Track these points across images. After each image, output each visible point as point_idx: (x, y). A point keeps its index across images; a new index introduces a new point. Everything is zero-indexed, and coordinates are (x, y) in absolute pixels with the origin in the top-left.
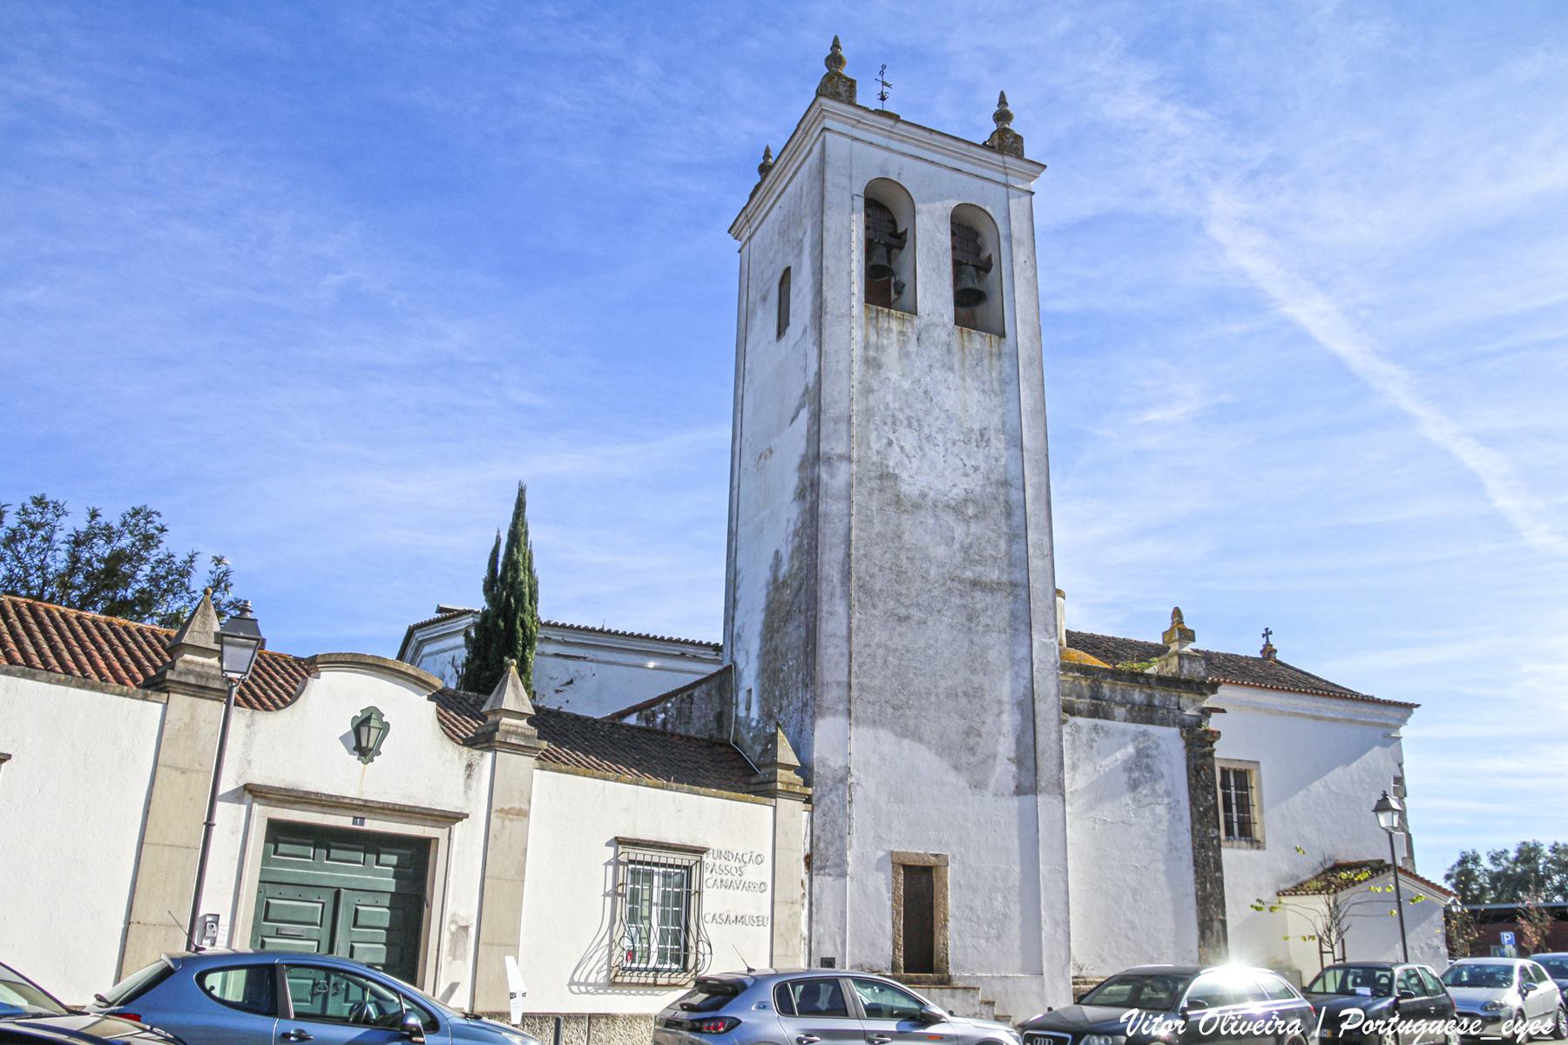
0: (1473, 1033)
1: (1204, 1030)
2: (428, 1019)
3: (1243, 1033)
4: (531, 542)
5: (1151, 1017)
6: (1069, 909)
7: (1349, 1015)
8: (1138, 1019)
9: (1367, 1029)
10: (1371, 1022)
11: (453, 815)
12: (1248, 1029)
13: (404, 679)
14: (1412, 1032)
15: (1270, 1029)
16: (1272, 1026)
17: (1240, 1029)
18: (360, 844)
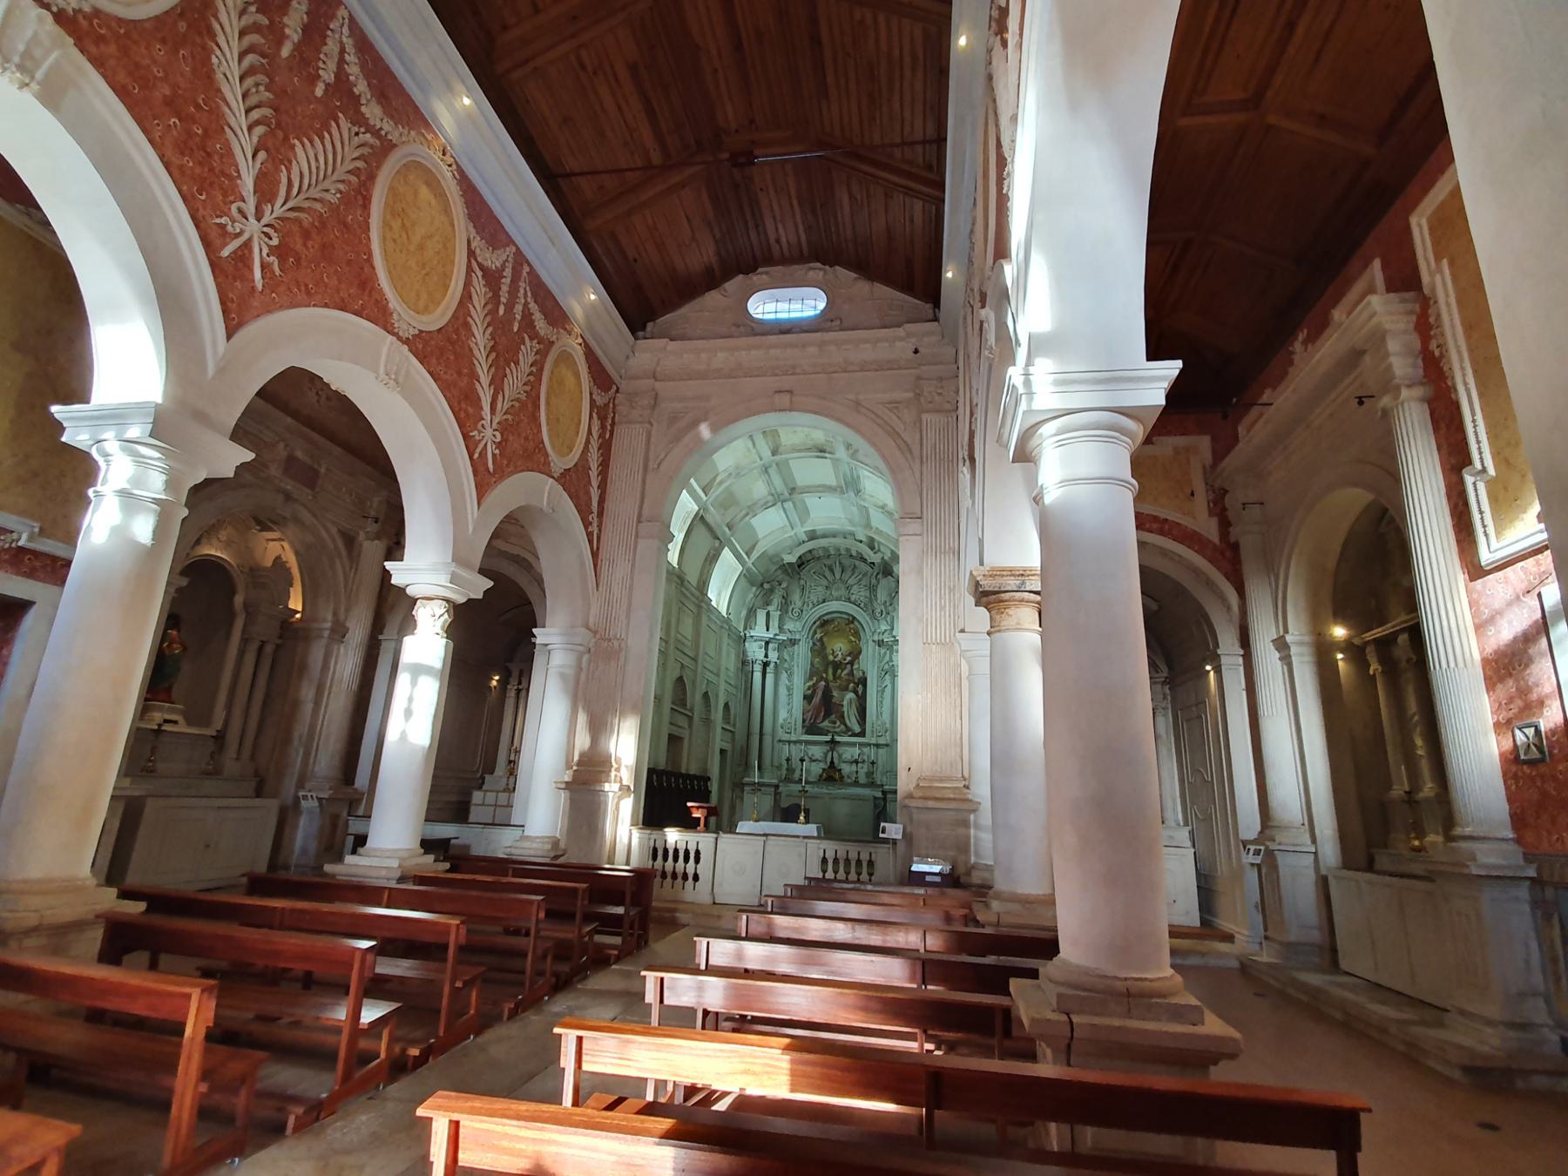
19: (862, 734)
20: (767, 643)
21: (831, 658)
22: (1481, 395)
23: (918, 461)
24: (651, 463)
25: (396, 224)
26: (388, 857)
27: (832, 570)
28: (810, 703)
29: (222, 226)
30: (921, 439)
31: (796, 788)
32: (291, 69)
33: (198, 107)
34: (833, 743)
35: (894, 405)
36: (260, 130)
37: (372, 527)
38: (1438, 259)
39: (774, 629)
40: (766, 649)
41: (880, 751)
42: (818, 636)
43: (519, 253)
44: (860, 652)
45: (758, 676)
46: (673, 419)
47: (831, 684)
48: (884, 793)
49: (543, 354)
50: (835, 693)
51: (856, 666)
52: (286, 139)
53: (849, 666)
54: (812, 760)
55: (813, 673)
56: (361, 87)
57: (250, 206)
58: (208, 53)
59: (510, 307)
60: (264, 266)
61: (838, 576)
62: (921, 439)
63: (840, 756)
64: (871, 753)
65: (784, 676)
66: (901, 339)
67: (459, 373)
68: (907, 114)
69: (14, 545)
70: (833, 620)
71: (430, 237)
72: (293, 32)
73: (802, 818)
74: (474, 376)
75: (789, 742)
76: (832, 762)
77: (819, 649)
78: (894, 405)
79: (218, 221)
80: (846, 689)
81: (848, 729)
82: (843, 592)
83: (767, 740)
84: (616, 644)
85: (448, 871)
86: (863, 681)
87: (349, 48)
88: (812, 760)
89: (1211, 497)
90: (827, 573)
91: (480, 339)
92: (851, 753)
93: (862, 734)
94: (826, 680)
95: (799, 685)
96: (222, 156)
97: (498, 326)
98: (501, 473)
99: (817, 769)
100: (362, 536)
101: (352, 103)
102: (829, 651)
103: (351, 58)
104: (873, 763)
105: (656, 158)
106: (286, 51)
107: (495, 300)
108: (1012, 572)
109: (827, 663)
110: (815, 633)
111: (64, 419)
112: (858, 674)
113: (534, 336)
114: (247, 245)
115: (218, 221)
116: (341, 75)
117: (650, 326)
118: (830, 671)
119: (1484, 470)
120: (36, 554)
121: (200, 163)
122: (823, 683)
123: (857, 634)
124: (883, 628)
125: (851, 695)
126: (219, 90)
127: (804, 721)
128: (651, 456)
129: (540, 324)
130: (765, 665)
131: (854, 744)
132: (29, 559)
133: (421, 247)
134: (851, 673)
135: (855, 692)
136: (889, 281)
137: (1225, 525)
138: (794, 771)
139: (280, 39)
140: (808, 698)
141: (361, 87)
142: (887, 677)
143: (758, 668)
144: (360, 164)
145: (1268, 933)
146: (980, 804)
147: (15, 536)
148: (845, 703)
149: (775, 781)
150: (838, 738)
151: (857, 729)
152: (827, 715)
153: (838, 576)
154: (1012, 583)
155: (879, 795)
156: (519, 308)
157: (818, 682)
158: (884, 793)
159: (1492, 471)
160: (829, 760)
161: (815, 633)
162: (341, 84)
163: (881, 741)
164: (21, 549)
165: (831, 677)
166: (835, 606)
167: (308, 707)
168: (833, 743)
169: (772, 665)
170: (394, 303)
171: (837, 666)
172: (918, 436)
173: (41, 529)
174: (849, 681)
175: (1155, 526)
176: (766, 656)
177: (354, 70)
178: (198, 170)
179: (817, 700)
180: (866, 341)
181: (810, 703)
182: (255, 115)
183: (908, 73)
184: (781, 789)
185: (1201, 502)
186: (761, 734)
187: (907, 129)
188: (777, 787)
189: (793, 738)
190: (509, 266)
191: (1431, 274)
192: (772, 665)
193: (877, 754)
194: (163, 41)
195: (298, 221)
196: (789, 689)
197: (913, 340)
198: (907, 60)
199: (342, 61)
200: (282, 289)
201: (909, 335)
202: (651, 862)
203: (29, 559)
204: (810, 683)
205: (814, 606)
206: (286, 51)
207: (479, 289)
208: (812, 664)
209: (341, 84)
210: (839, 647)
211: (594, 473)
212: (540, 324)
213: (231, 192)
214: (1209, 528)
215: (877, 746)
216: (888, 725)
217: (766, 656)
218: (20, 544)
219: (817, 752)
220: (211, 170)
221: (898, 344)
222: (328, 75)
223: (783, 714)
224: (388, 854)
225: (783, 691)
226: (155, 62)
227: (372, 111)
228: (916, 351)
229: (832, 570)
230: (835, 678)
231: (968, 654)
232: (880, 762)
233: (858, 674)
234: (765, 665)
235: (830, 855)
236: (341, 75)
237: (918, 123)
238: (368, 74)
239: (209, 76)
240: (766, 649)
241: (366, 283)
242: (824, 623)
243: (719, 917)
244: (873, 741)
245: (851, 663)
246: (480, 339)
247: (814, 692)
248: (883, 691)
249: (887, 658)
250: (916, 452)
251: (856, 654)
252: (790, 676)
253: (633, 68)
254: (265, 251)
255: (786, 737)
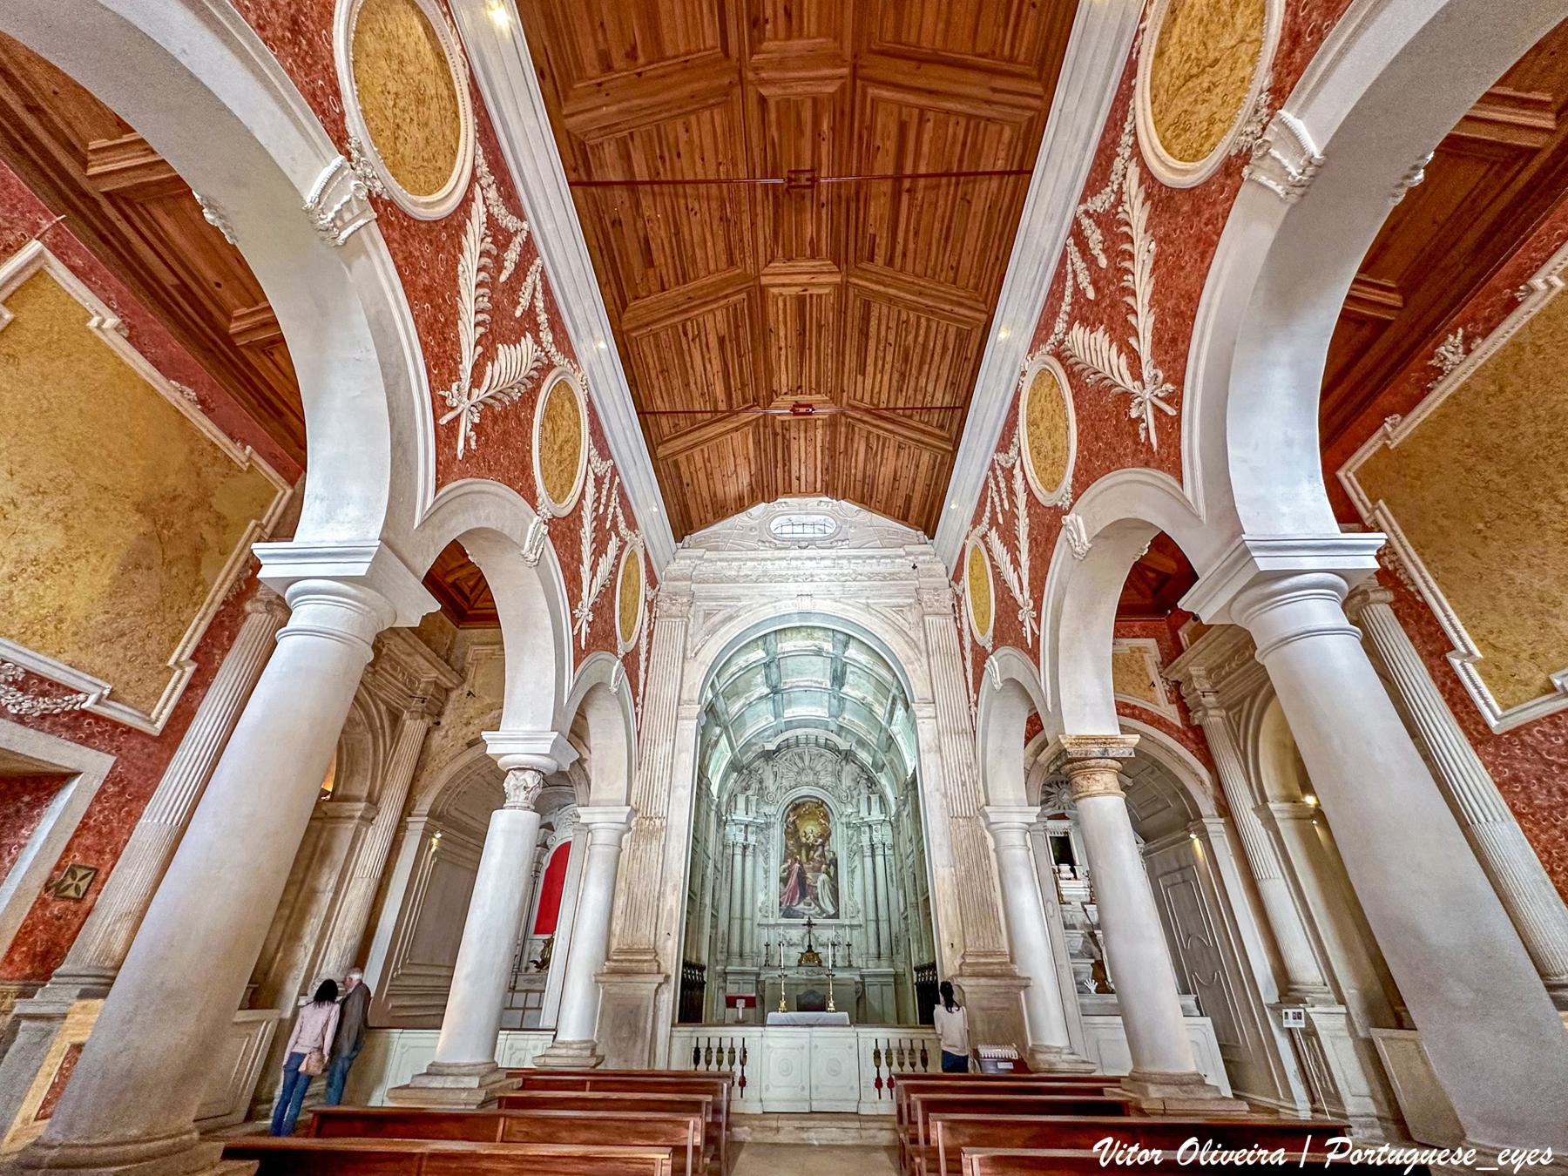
0: (1467, 1163)
1: (1183, 1161)
2: (669, 1149)
3: (1224, 1163)
4: (1027, 326)
5: (1125, 1146)
6: (1538, 970)
7: (1335, 1144)
8: (1112, 1147)
9: (1355, 1158)
10: (1359, 1151)
11: (622, 348)
12: (1230, 1159)
13: (522, 908)
14: (1539, 1163)
15: (1252, 1159)
16: (1255, 1156)
17: (1222, 1159)
18: (20, 246)
19: (836, 916)
20: (746, 826)
21: (804, 840)
22: (1448, 597)
23: (924, 655)
24: (689, 652)
25: (549, 427)
26: (465, 1075)
27: (802, 759)
28: (785, 885)
29: (444, 398)
30: (926, 636)
31: (776, 973)
32: (503, 292)
33: (444, 300)
34: (810, 924)
35: (899, 609)
36: (481, 330)
37: (416, 705)
38: (1374, 501)
39: (752, 814)
40: (746, 833)
41: (855, 933)
42: (791, 819)
43: (614, 467)
44: (830, 834)
45: (738, 858)
46: (708, 615)
47: (805, 866)
48: (862, 976)
49: (621, 549)
50: (809, 875)
51: (827, 848)
52: (494, 341)
53: (820, 848)
54: (790, 945)
55: (787, 855)
56: (543, 318)
57: (466, 383)
58: (457, 262)
59: (607, 506)
60: (467, 440)
61: (807, 763)
62: (926, 636)
63: (817, 939)
64: (846, 935)
65: (761, 859)
66: (901, 557)
67: (572, 558)
68: (930, 388)
69: (76, 708)
70: (804, 804)
71: (567, 442)
72: (509, 267)
73: (783, 1004)
74: (580, 561)
75: (768, 926)
76: (810, 946)
77: (792, 832)
78: (899, 609)
79: (442, 393)
80: (819, 870)
81: (823, 911)
82: (811, 777)
83: (747, 924)
84: (658, 822)
85: (522, 1088)
86: (834, 862)
87: (539, 288)
88: (790, 945)
89: (1167, 688)
90: (798, 761)
91: (587, 532)
92: (827, 935)
93: (836, 916)
94: (800, 862)
95: (775, 867)
96: (453, 343)
97: (599, 520)
98: (588, 650)
99: (795, 953)
100: (406, 715)
101: (535, 330)
102: (801, 833)
103: (539, 295)
104: (849, 945)
105: (722, 406)
106: (503, 278)
107: (598, 500)
108: (1095, 740)
109: (800, 845)
110: (788, 816)
111: (265, 556)
112: (829, 856)
113: (618, 535)
114: (457, 418)
115: (442, 393)
116: (532, 306)
117: (687, 538)
118: (804, 853)
119: (1470, 653)
120: (98, 718)
121: (439, 345)
122: (797, 865)
123: (826, 816)
124: (850, 811)
125: (823, 877)
126: (459, 292)
127: (781, 904)
128: (689, 646)
129: (622, 525)
130: (745, 848)
131: (830, 926)
132: (89, 724)
133: (561, 448)
134: (823, 855)
135: (828, 873)
136: (886, 512)
137: (1185, 710)
138: (773, 956)
139: (500, 269)
140: (784, 881)
141: (543, 318)
142: (856, 858)
143: (738, 851)
144: (534, 373)
145: (1317, 1105)
146: (1029, 979)
147: (81, 697)
148: (819, 885)
149: (756, 969)
150: (814, 921)
151: (831, 911)
152: (803, 896)
153: (807, 763)
154: (1096, 750)
155: (858, 979)
156: (611, 510)
157: (792, 864)
158: (862, 976)
159: (1478, 654)
160: (806, 944)
161: (788, 816)
162: (531, 312)
163: (855, 922)
164: (84, 713)
165: (804, 859)
166: (805, 791)
167: (325, 899)
168: (810, 924)
169: (751, 848)
170: (540, 489)
171: (810, 848)
172: (922, 635)
173: (112, 692)
174: (821, 863)
175: (1128, 711)
176: (746, 839)
177: (540, 304)
178: (436, 350)
179: (792, 881)
180: (872, 557)
181: (785, 885)
182: (481, 317)
183: (936, 358)
184: (762, 978)
185: (1161, 692)
186: (742, 919)
187: (928, 398)
188: (758, 975)
189: (772, 921)
190: (609, 475)
191: (1371, 512)
192: (751, 848)
193: (851, 935)
194: (431, 242)
195: (491, 407)
196: (766, 872)
197: (911, 558)
198: (938, 350)
199: (533, 297)
200: (474, 460)
201: (909, 554)
202: (693, 1067)
203: (89, 724)
204: (786, 865)
205: (787, 791)
206: (503, 278)
207: (591, 490)
208: (786, 847)
209: (531, 312)
210: (810, 829)
211: (643, 657)
212: (622, 525)
213: (454, 374)
214: (1171, 714)
215: (851, 926)
216: (860, 906)
217: (746, 839)
218: (83, 706)
219: (796, 935)
220: (445, 352)
221: (897, 560)
222: (524, 301)
223: (761, 897)
224: (465, 1070)
225: (760, 873)
226: (423, 256)
227: (547, 337)
228: (914, 567)
229: (802, 759)
230: (808, 860)
231: (994, 827)
232: (854, 944)
233: (829, 856)
234: (745, 848)
235: (882, 1047)
236: (532, 306)
237: (939, 395)
238: (547, 310)
239: (455, 279)
240: (746, 833)
241: (526, 469)
242: (796, 807)
243: (778, 1129)
244: (847, 922)
245: (823, 845)
246: (587, 532)
247: (789, 874)
248: (853, 872)
249: (855, 839)
250: (923, 647)
251: (826, 836)
252: (766, 859)
253: (721, 341)
254: (469, 426)
255: (765, 921)
